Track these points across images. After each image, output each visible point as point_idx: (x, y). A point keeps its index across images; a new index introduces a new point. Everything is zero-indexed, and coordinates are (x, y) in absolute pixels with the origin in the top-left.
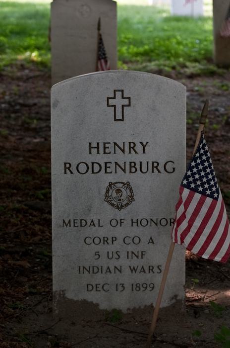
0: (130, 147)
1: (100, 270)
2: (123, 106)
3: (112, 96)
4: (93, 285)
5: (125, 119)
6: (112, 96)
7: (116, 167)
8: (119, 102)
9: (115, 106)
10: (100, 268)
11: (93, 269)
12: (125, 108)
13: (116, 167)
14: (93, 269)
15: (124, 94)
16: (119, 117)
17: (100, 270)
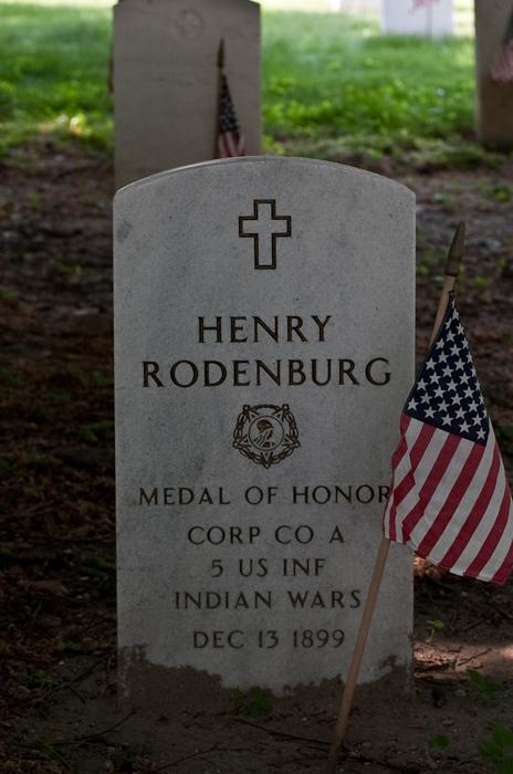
0: (290, 328)
1: (223, 601)
2: (274, 236)
3: (250, 213)
4: (208, 635)
5: (278, 264)
6: (250, 213)
7: (258, 371)
8: (265, 226)
9: (256, 236)
10: (223, 596)
11: (208, 598)
12: (279, 240)
13: (258, 371)
14: (208, 598)
15: (277, 209)
16: (265, 259)
17: (223, 601)
